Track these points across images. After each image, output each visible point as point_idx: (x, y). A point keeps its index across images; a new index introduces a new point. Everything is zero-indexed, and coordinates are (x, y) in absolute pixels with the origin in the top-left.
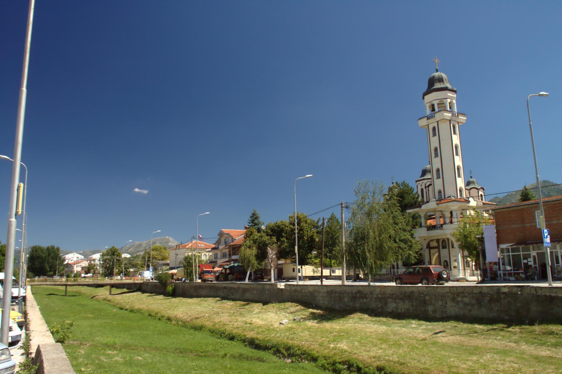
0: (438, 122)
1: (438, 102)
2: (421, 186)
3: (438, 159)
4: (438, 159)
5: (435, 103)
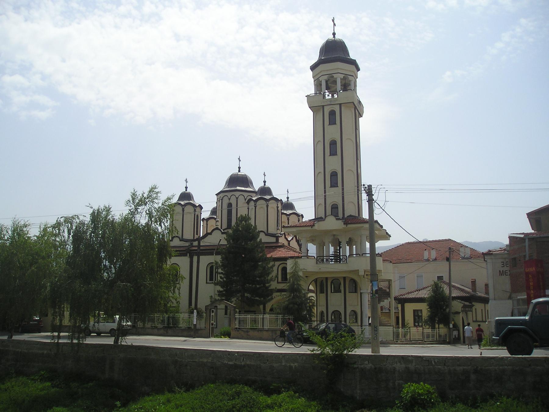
0: (340, 104)
2: (229, 199)
3: (338, 158)
4: (338, 158)
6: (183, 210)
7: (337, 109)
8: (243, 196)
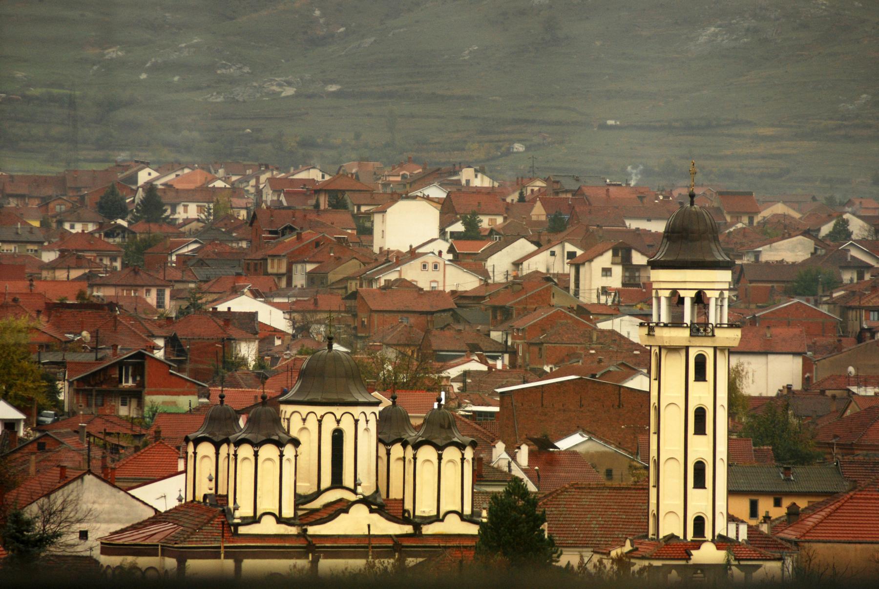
1: (693, 294)
5: (688, 296)
6: (256, 455)
7: (709, 354)
8: (351, 416)
